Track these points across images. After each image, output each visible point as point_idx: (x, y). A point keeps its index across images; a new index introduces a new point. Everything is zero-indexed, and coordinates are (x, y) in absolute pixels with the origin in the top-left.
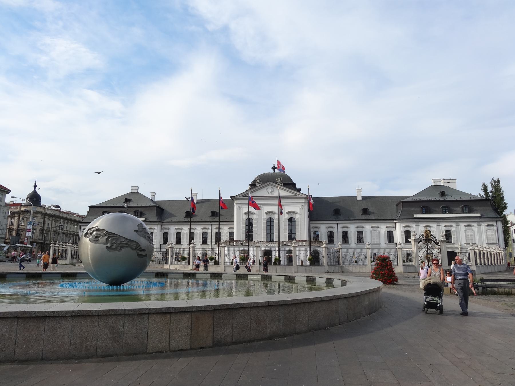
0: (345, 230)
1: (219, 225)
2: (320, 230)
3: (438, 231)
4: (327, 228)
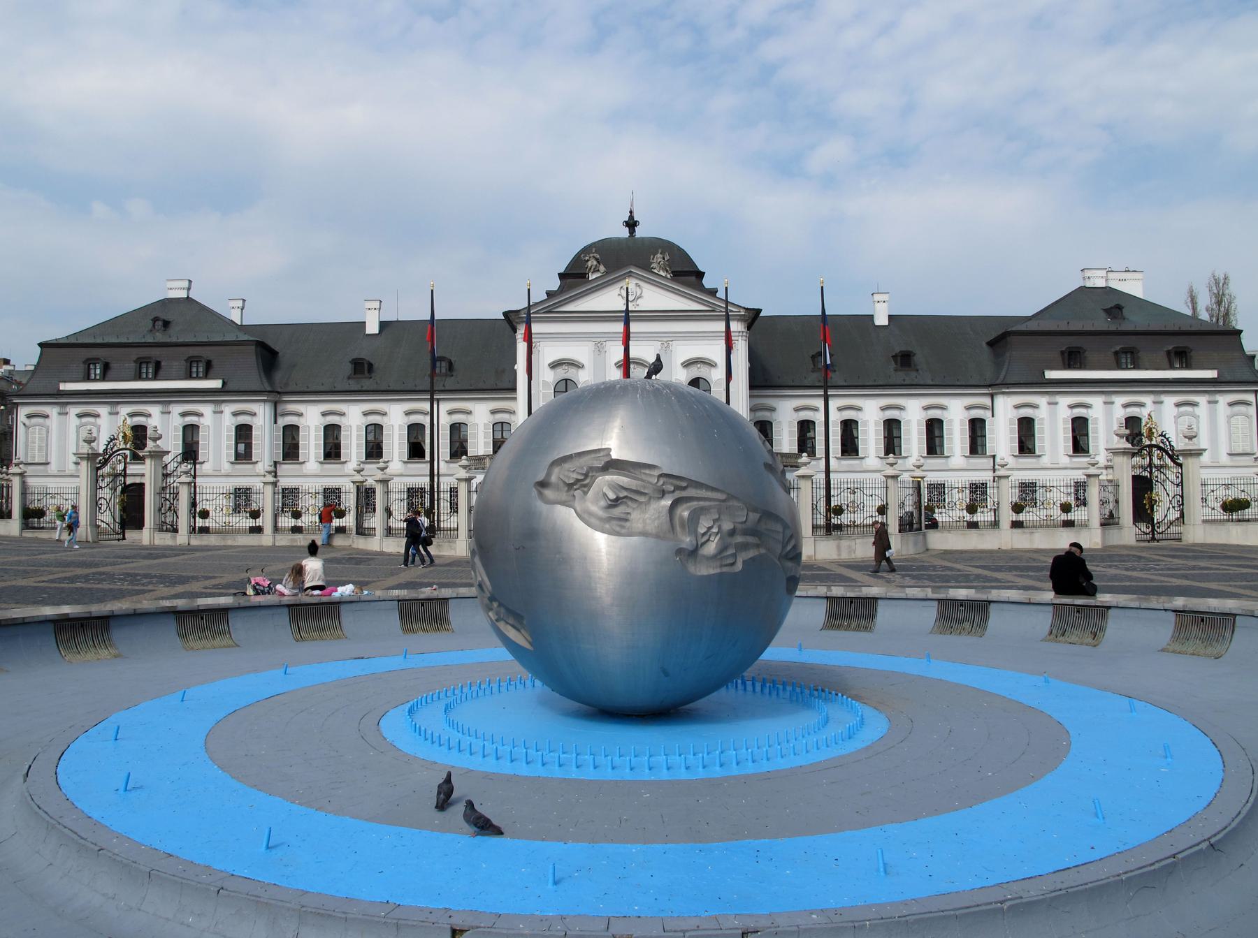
0: (458, 418)
4: (968, 408)
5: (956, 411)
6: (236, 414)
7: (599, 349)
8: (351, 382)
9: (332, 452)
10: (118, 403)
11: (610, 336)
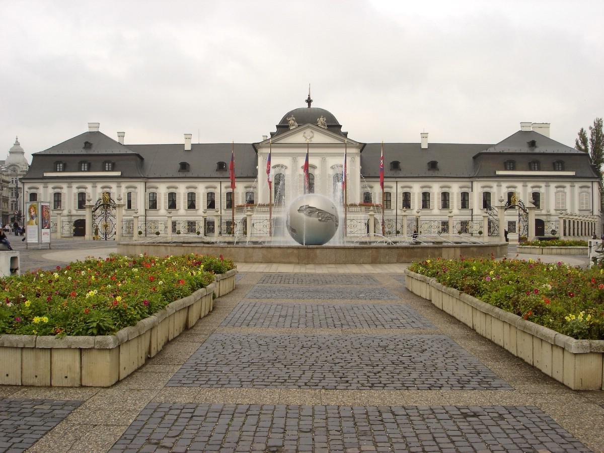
2: (137, 190)
3: (523, 192)
4: (422, 187)
5: (455, 189)
6: (54, 188)
7: (295, 161)
8: (218, 173)
9: (445, 204)
10: (72, 182)
11: (300, 155)
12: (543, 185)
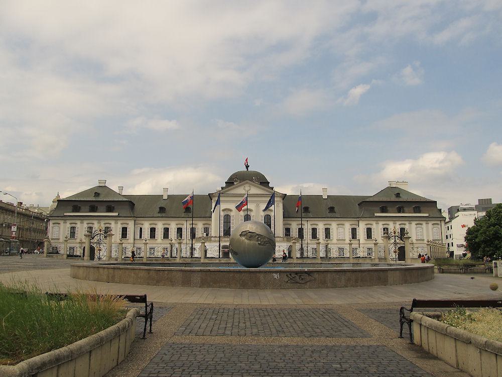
0: (314, 227)
1: (193, 220)
6: (71, 224)
7: (258, 206)
12: (407, 223)
